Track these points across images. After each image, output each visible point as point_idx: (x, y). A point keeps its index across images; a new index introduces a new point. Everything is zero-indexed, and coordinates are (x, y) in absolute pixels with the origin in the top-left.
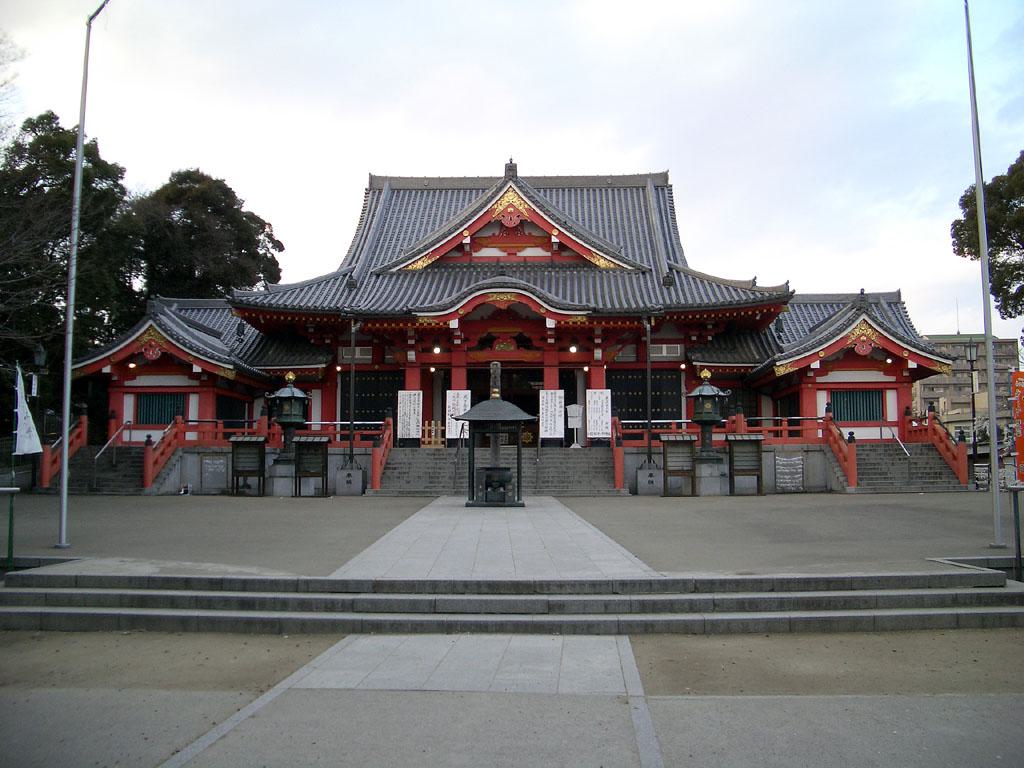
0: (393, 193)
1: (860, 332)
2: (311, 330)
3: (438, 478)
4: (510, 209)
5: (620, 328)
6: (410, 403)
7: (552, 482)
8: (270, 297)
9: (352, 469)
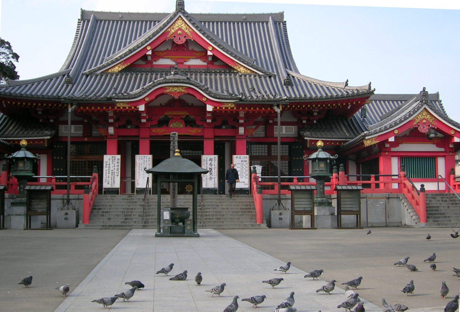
0: (97, 22)
1: (423, 119)
2: (40, 113)
3: (131, 215)
4: (180, 32)
5: (260, 113)
6: (111, 163)
7: (212, 219)
8: (10, 88)
9: (68, 209)
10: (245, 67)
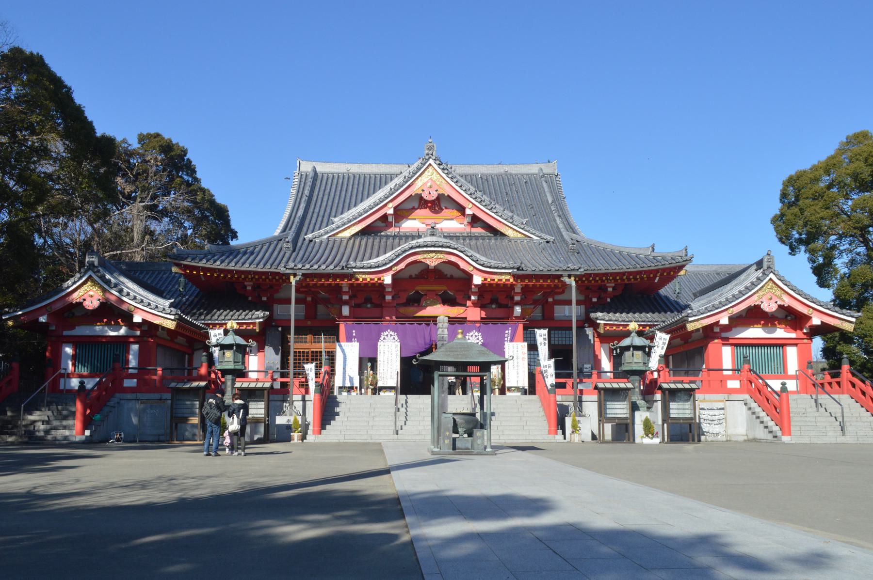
2: (249, 288)
10: (514, 230)
